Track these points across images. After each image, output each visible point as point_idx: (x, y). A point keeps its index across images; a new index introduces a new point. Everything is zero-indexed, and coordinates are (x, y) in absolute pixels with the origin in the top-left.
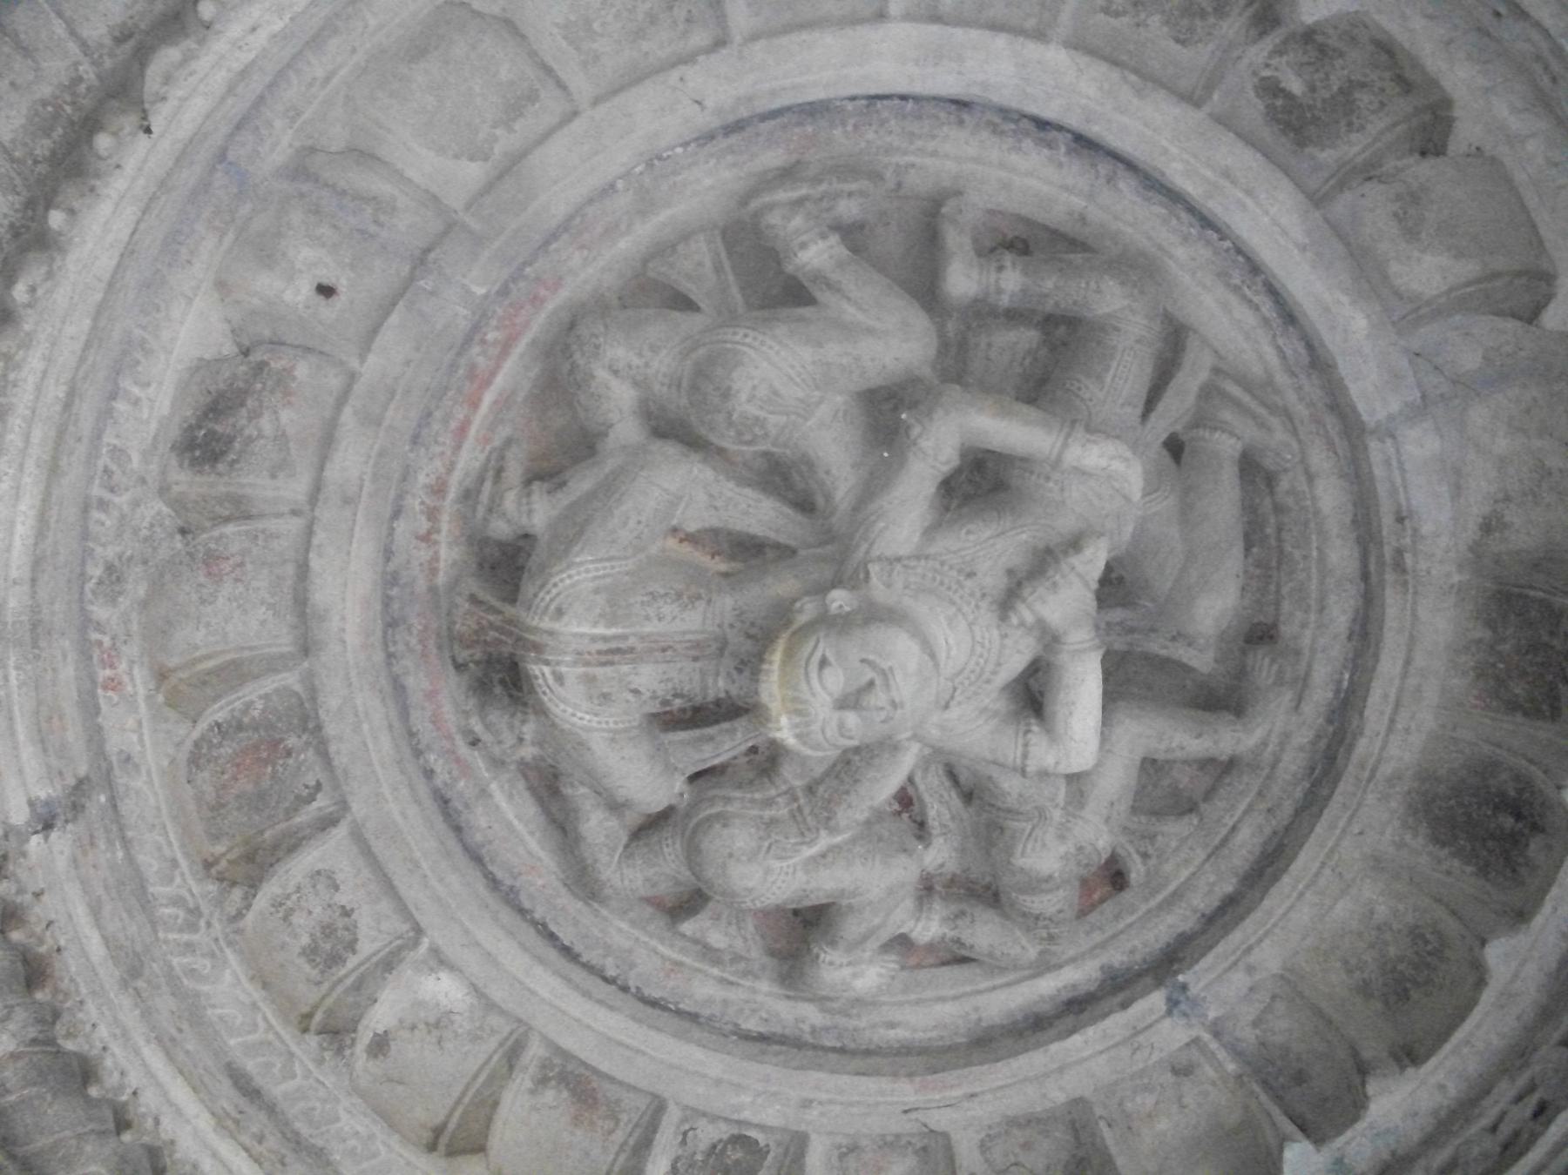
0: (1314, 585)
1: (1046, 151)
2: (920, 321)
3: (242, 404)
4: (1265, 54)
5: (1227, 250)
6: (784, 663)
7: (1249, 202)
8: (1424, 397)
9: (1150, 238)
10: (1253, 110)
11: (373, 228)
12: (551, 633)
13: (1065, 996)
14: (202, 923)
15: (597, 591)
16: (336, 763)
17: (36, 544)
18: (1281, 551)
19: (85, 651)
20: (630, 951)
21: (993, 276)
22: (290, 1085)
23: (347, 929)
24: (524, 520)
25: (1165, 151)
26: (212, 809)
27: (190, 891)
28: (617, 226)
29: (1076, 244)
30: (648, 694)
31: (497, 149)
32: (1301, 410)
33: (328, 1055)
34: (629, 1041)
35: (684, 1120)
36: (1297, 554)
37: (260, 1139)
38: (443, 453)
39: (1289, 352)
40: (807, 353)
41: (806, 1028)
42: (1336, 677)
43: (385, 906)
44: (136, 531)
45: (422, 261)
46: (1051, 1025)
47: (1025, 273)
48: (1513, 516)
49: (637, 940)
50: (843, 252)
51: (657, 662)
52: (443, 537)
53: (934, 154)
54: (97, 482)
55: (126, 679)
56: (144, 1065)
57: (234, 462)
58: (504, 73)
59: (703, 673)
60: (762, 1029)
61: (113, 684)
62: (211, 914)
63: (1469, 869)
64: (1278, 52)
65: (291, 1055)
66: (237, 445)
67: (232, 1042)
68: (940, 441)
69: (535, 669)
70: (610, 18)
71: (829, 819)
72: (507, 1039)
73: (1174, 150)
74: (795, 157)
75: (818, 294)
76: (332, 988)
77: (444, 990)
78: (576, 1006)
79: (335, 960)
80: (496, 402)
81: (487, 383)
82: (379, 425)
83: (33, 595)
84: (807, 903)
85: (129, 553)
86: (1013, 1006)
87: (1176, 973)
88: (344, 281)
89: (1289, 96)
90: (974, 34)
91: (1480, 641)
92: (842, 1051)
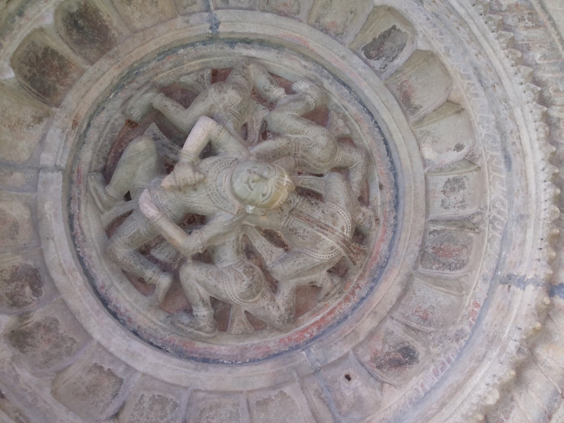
0: (107, 130)
1: (118, 305)
2: (182, 276)
3: (390, 359)
4: (32, 305)
5: (79, 247)
6: (275, 201)
7: (62, 262)
8: (39, 172)
9: (101, 263)
10: (45, 289)
11: (325, 389)
12: (338, 244)
13: (249, 46)
14: (491, 218)
15: (318, 249)
16: (421, 238)
17: (477, 367)
18: (112, 147)
19: (479, 320)
20: (368, 133)
21: (154, 278)
22: (494, 153)
23: (447, 187)
24: (328, 278)
25: (80, 290)
26: (466, 247)
27: (489, 230)
28: (255, 348)
29: (124, 272)
30: (320, 209)
31: (277, 392)
32: (82, 186)
33: (477, 156)
34: (384, 107)
35: (383, 72)
36: (107, 143)
37: (514, 143)
38: (341, 309)
39: (77, 207)
40: (220, 286)
41: (330, 81)
42: (115, 98)
43: (431, 187)
44: (443, 347)
45: (316, 371)
46: (258, 39)
47: (144, 274)
48: (29, 119)
49: (364, 135)
50: (194, 308)
51: (313, 218)
52: (353, 284)
53: (152, 322)
54: (447, 369)
55: (471, 304)
56: (537, 189)
57: (402, 343)
58: (262, 415)
59: (301, 206)
60: (343, 87)
61: (476, 305)
62: (487, 218)
63: (101, 14)
64: (27, 303)
65: (488, 163)
66: (398, 348)
67: (504, 176)
68: (193, 242)
69: (348, 235)
70: (223, 415)
71: (289, 143)
72: (419, 127)
73: (77, 289)
74: (193, 342)
75: (208, 299)
76: (462, 173)
77: (429, 153)
78: (393, 127)
79: (456, 180)
80: (317, 315)
81: (316, 322)
82: (354, 330)
83: (486, 352)
84: (309, 121)
85: (449, 341)
86: (266, 52)
87: (211, 34)
88: (341, 378)
89: (32, 287)
90: (118, 355)
91: (61, 85)
92: (324, 67)
